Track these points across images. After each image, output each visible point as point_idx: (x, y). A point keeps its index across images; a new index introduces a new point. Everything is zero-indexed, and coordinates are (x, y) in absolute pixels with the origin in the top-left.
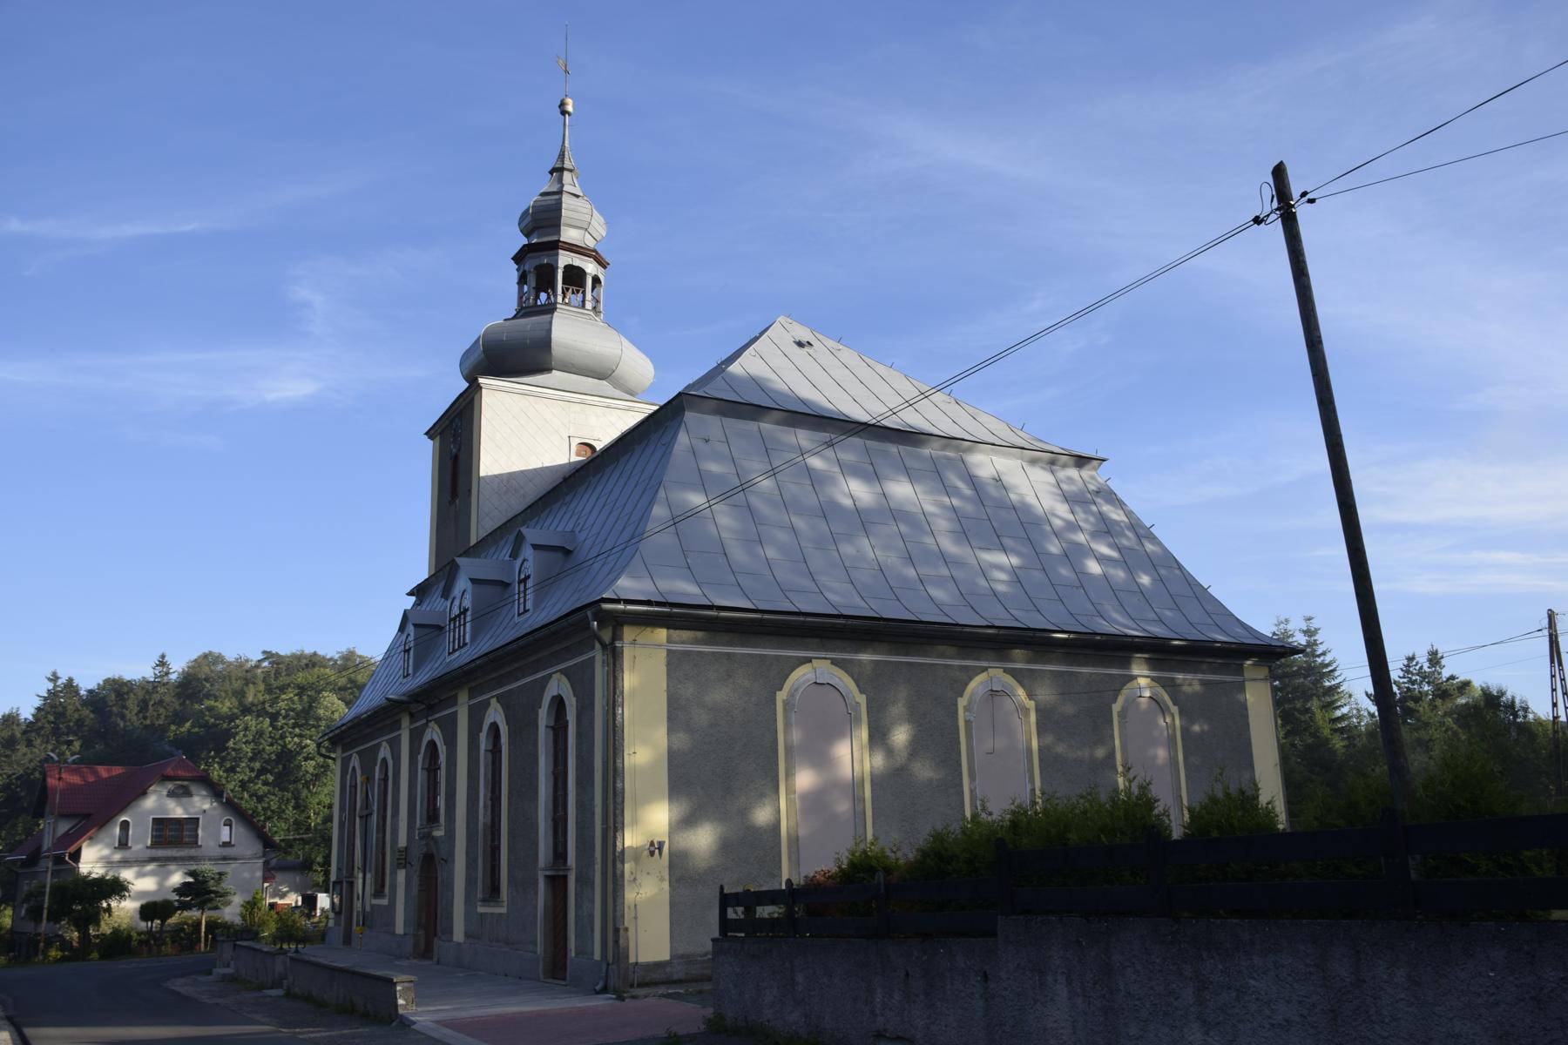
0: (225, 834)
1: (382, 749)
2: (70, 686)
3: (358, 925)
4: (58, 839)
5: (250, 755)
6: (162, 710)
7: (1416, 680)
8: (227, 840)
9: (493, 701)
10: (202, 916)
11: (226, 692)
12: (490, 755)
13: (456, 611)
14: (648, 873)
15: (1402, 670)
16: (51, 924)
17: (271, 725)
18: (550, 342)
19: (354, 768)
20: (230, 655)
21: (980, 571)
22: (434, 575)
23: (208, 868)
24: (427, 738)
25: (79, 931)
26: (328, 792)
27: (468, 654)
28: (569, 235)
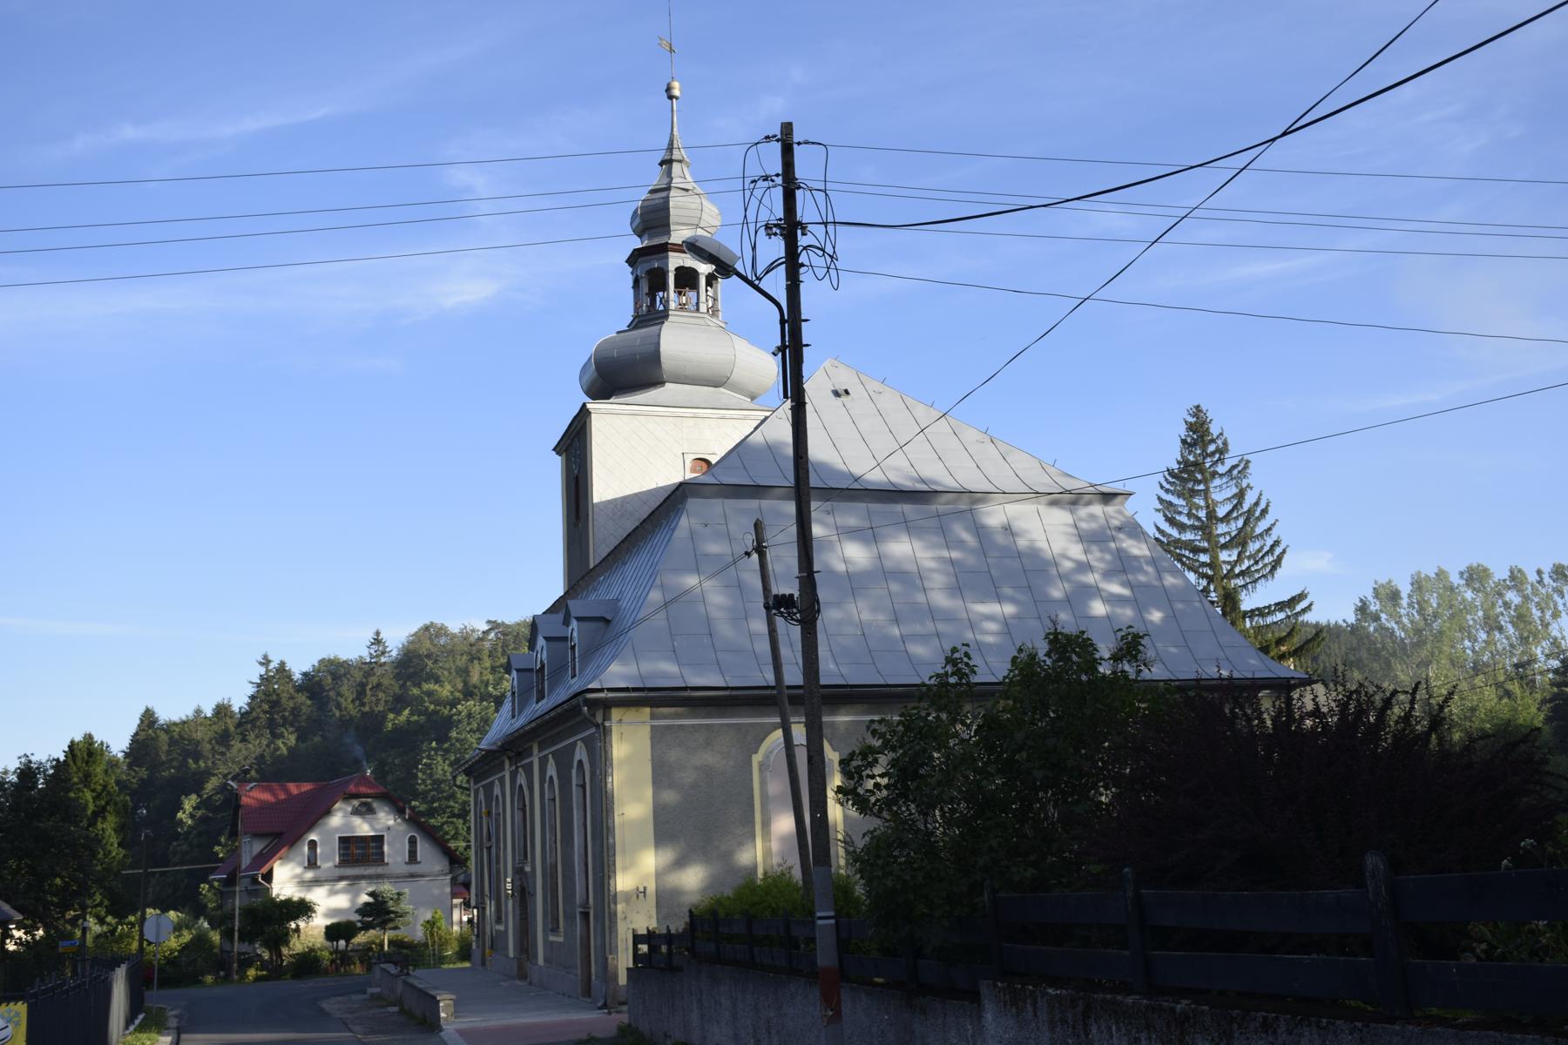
1: (578, 749)
2: (282, 669)
6: (381, 695)
11: (449, 670)
14: (638, 912)
20: (454, 627)
23: (387, 888)
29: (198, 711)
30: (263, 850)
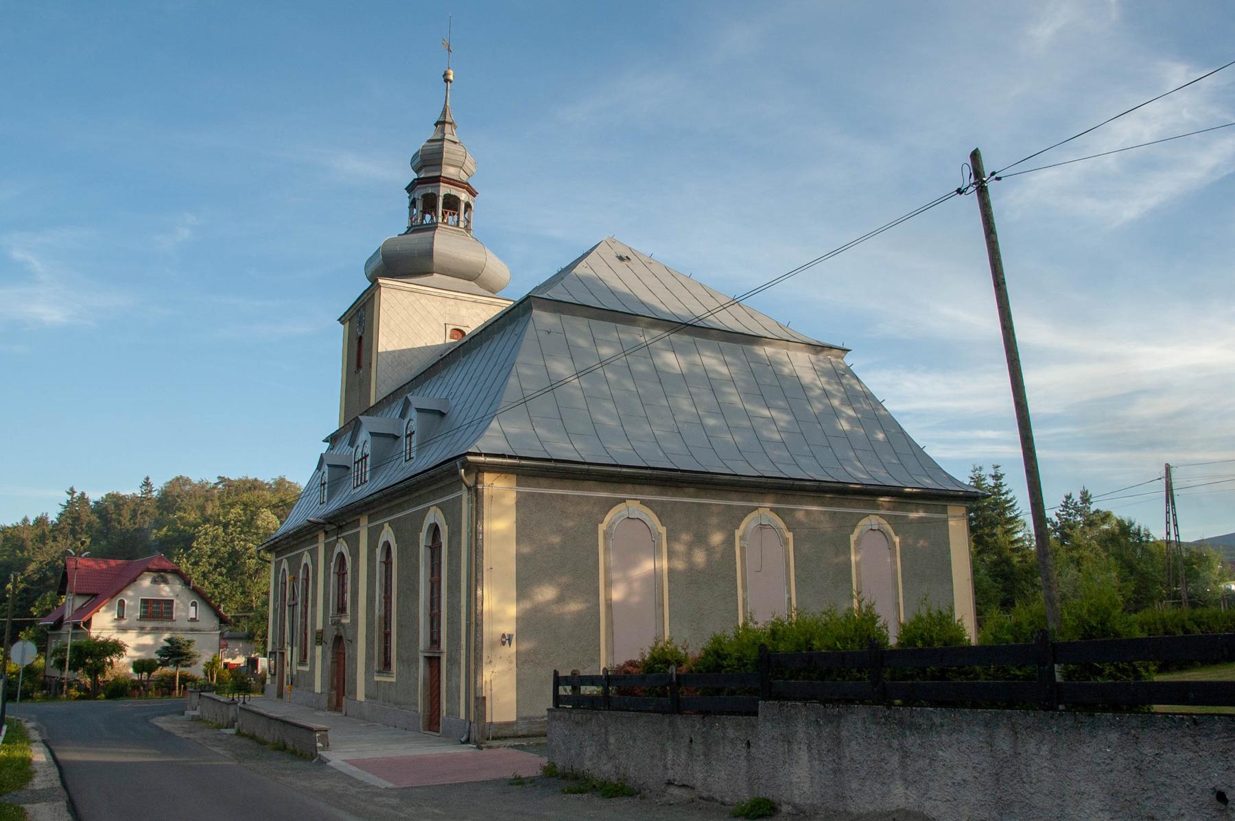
0: (192, 612)
1: (304, 557)
3: (287, 684)
4: (75, 611)
5: (209, 553)
7: (1072, 513)
8: (194, 617)
9: (386, 525)
10: (179, 671)
12: (383, 565)
13: (359, 456)
15: (1062, 506)
16: (72, 671)
17: (224, 531)
18: (433, 253)
19: (284, 570)
20: (195, 479)
21: (656, 321)
22: (343, 427)
23: (183, 637)
24: (337, 551)
25: (91, 678)
26: (269, 579)
27: (367, 489)
28: (449, 171)
29: (26, 520)
30: (83, 605)
